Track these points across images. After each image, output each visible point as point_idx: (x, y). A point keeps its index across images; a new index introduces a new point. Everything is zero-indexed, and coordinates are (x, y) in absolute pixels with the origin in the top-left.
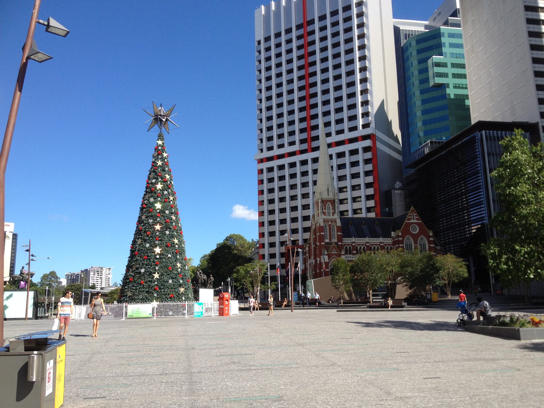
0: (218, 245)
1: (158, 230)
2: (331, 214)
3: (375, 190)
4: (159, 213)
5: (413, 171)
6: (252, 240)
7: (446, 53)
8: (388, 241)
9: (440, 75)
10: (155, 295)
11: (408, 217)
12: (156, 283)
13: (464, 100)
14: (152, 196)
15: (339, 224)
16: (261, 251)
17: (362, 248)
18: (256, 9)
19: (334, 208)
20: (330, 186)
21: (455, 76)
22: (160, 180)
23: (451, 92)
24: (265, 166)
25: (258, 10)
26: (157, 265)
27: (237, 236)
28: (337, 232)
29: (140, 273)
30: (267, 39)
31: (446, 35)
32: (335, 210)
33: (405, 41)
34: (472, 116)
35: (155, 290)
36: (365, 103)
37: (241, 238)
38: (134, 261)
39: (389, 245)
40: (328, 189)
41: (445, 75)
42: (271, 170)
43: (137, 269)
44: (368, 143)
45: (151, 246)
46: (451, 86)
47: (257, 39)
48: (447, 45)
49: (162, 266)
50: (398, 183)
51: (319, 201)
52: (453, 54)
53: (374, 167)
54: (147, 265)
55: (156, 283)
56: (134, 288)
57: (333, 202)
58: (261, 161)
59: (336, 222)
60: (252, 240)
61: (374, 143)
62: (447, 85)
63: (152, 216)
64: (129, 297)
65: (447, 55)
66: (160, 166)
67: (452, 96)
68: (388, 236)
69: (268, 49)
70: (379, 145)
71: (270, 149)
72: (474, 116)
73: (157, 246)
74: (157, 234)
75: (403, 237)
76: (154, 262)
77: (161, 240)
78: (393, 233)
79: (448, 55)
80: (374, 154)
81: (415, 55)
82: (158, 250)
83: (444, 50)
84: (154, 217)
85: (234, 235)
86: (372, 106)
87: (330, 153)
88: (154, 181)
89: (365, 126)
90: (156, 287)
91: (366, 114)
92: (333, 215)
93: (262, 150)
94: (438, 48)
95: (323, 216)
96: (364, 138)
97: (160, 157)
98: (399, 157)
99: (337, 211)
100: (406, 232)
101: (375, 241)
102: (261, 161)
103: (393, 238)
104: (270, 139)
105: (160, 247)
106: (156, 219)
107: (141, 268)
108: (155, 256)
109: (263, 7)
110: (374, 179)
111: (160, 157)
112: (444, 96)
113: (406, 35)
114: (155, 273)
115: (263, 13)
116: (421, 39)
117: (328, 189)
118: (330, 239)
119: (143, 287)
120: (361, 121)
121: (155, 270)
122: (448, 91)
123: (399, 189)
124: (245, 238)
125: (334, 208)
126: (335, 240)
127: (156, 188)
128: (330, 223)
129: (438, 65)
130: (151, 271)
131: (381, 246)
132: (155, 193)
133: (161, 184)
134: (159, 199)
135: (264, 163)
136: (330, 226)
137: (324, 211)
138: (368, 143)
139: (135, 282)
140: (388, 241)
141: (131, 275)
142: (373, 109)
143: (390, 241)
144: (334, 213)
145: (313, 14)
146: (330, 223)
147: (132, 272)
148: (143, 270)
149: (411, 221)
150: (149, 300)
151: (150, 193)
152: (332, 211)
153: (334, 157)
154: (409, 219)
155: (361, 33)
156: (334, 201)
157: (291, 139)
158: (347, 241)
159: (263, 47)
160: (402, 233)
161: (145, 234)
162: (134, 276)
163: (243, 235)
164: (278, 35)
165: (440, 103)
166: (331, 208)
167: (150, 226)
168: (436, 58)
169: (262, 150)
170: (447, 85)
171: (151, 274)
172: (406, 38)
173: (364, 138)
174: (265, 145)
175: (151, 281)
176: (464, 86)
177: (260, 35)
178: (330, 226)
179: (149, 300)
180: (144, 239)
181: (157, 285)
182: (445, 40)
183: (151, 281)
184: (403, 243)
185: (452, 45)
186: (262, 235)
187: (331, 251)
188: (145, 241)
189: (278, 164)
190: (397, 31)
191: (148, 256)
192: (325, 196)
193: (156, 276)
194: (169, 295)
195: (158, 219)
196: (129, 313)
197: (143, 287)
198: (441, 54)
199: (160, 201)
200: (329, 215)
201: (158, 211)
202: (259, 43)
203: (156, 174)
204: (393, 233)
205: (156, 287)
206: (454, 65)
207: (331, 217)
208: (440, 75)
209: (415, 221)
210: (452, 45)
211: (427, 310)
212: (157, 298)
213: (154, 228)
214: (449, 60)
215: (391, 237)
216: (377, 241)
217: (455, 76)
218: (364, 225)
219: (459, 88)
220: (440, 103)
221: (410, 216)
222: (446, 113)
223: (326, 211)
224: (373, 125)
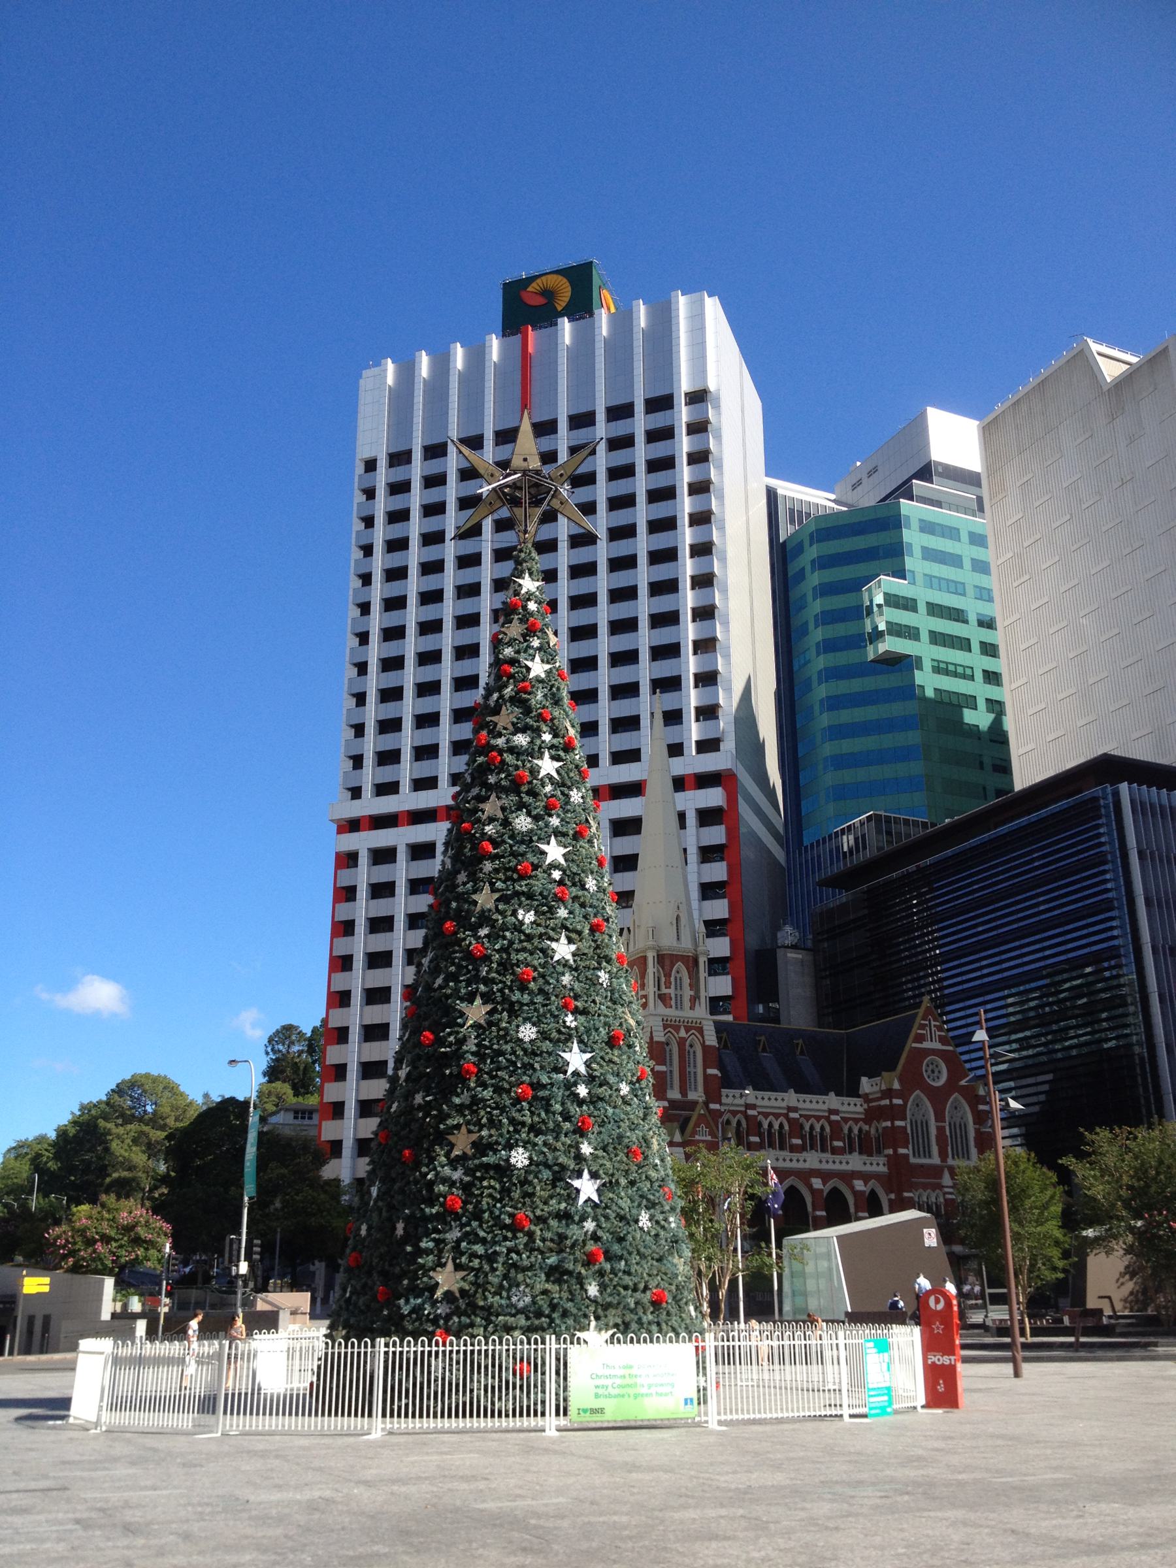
0: (83, 1108)
1: (564, 963)
2: (687, 1004)
3: (733, 945)
4: (561, 883)
5: (843, 897)
6: (206, 1096)
7: (913, 572)
8: (852, 1108)
9: (897, 630)
10: (593, 1290)
11: (916, 1030)
12: (590, 1225)
13: (961, 707)
14: (521, 805)
15: (711, 1039)
16: (334, 1054)
17: (776, 1127)
18: (368, 367)
19: (695, 985)
20: (683, 907)
21: (937, 638)
22: (547, 737)
23: (928, 682)
24: (364, 842)
25: (376, 370)
26: (581, 1132)
27: (155, 1080)
28: (706, 1067)
29: (504, 1170)
30: (400, 458)
31: (915, 524)
32: (697, 991)
33: (791, 529)
34: (1017, 750)
35: (590, 1260)
36: (707, 679)
37: (170, 1088)
38: (460, 1109)
39: (856, 1121)
40: (678, 918)
41: (911, 633)
42: (383, 856)
43: (481, 1148)
44: (714, 797)
45: (544, 1035)
46: (927, 665)
47: (365, 453)
48: (917, 551)
49: (608, 1140)
50: (788, 929)
51: (651, 956)
52: (931, 577)
53: (731, 871)
54: (534, 1129)
55: (590, 1225)
56: (479, 1249)
57: (692, 963)
58: (352, 825)
59: (700, 1030)
60: (206, 1096)
61: (732, 799)
62: (917, 662)
63: (530, 896)
64: (449, 1296)
65: (919, 578)
66: (539, 680)
67: (930, 693)
68: (852, 1090)
69: (399, 488)
70: (744, 809)
71: (387, 789)
72: (1021, 751)
73: (569, 1038)
74: (566, 979)
75: (904, 1094)
76: (567, 1117)
77: (584, 1012)
78: (864, 1080)
79: (919, 579)
80: (732, 833)
81: (825, 569)
82: (576, 1059)
83: (910, 563)
84: (545, 906)
85: (147, 1076)
86: (729, 690)
87: (680, 808)
88: (521, 740)
89: (708, 746)
90: (591, 1247)
91: (708, 712)
92: (692, 1008)
93: (356, 793)
94: (892, 557)
95: (662, 1009)
96: (704, 780)
97: (536, 643)
98: (779, 854)
99: (703, 994)
100: (913, 1080)
101: (814, 1106)
102: (352, 825)
103: (866, 1098)
104: (389, 757)
105: (584, 1047)
106: (552, 911)
107: (510, 1147)
108: (569, 1086)
109: (390, 367)
110: (732, 908)
111: (536, 643)
112: (910, 691)
113: (792, 511)
114: (579, 1175)
115: (390, 380)
116: (828, 529)
117: (678, 918)
118: (684, 1092)
119: (530, 1248)
120: (694, 731)
121: (579, 1158)
122: (920, 678)
123: (794, 947)
124: (182, 1089)
125: (695, 985)
126: (697, 1095)
127: (534, 771)
128: (683, 1033)
129: (893, 601)
130: (563, 1159)
131: (831, 1123)
132: (533, 793)
133: (555, 758)
134: (555, 821)
135: (363, 834)
136: (681, 1042)
137: (664, 991)
138: (714, 797)
139: (477, 1215)
140: (851, 1107)
141: (445, 1180)
142: (728, 700)
143: (859, 1109)
144: (694, 999)
145: (555, 405)
146: (683, 1033)
147: (453, 1163)
148: (519, 1158)
149: (926, 1045)
150: (565, 1314)
151: (507, 791)
152: (688, 993)
153: (691, 820)
154: (920, 1038)
155: (701, 478)
156: (696, 961)
157: (425, 769)
158: (733, 1099)
159: (382, 477)
160: (901, 1081)
161: (509, 979)
162: (466, 1188)
163: (176, 1077)
164: (435, 451)
165: (896, 709)
166: (686, 981)
167: (529, 938)
168: (888, 583)
169: (356, 793)
170: (917, 662)
171: (560, 1176)
172: (792, 522)
173: (704, 780)
174: (369, 775)
175: (565, 1217)
176: (968, 672)
177: (374, 439)
178: (681, 1042)
179: (565, 1314)
180: (505, 999)
181: (595, 1238)
182: (911, 536)
183: (565, 1217)
184: (904, 1119)
185: (930, 555)
186: (340, 999)
187: (694, 1133)
188: (514, 1011)
189: (412, 840)
190: (772, 495)
191: (537, 1086)
192: (668, 941)
193: (587, 1188)
194: (646, 1288)
195: (562, 913)
196: (581, 1393)
197: (530, 1248)
198: (901, 573)
199: (558, 833)
200: (679, 1006)
201: (556, 875)
202: (371, 465)
203: (527, 710)
204: (864, 1080)
205: (591, 1247)
206: (935, 610)
207: (687, 1014)
208: (897, 630)
209: (937, 1045)
210: (930, 555)
211: (1111, 1360)
212: (607, 1307)
213: (546, 953)
214: (924, 595)
215: (859, 1096)
216: (821, 1106)
217: (937, 638)
218: (764, 1050)
219: (947, 672)
220: (896, 709)
221: (922, 1027)
222: (913, 737)
223: (672, 991)
224: (729, 745)
